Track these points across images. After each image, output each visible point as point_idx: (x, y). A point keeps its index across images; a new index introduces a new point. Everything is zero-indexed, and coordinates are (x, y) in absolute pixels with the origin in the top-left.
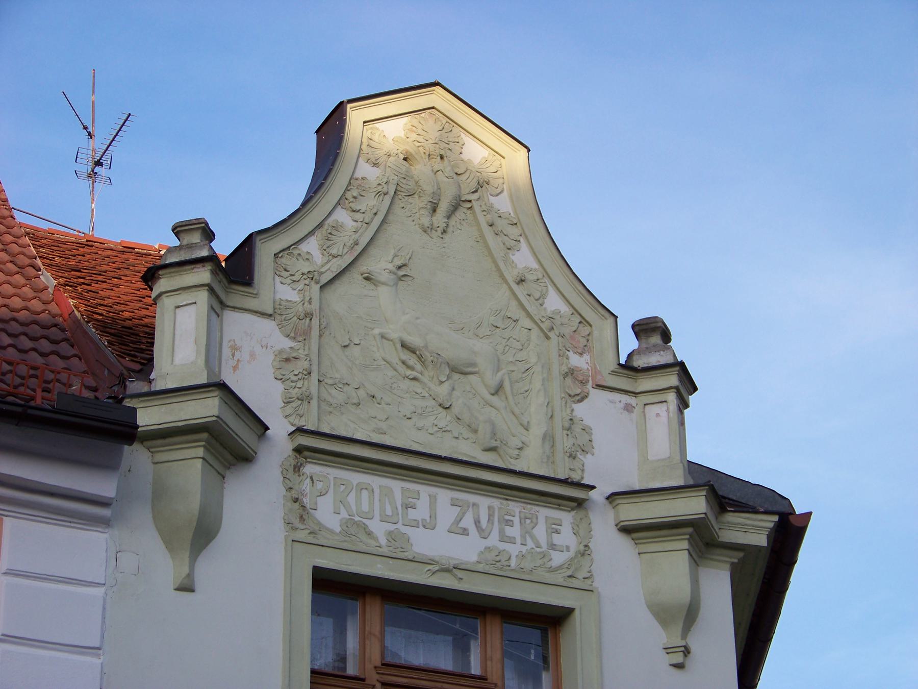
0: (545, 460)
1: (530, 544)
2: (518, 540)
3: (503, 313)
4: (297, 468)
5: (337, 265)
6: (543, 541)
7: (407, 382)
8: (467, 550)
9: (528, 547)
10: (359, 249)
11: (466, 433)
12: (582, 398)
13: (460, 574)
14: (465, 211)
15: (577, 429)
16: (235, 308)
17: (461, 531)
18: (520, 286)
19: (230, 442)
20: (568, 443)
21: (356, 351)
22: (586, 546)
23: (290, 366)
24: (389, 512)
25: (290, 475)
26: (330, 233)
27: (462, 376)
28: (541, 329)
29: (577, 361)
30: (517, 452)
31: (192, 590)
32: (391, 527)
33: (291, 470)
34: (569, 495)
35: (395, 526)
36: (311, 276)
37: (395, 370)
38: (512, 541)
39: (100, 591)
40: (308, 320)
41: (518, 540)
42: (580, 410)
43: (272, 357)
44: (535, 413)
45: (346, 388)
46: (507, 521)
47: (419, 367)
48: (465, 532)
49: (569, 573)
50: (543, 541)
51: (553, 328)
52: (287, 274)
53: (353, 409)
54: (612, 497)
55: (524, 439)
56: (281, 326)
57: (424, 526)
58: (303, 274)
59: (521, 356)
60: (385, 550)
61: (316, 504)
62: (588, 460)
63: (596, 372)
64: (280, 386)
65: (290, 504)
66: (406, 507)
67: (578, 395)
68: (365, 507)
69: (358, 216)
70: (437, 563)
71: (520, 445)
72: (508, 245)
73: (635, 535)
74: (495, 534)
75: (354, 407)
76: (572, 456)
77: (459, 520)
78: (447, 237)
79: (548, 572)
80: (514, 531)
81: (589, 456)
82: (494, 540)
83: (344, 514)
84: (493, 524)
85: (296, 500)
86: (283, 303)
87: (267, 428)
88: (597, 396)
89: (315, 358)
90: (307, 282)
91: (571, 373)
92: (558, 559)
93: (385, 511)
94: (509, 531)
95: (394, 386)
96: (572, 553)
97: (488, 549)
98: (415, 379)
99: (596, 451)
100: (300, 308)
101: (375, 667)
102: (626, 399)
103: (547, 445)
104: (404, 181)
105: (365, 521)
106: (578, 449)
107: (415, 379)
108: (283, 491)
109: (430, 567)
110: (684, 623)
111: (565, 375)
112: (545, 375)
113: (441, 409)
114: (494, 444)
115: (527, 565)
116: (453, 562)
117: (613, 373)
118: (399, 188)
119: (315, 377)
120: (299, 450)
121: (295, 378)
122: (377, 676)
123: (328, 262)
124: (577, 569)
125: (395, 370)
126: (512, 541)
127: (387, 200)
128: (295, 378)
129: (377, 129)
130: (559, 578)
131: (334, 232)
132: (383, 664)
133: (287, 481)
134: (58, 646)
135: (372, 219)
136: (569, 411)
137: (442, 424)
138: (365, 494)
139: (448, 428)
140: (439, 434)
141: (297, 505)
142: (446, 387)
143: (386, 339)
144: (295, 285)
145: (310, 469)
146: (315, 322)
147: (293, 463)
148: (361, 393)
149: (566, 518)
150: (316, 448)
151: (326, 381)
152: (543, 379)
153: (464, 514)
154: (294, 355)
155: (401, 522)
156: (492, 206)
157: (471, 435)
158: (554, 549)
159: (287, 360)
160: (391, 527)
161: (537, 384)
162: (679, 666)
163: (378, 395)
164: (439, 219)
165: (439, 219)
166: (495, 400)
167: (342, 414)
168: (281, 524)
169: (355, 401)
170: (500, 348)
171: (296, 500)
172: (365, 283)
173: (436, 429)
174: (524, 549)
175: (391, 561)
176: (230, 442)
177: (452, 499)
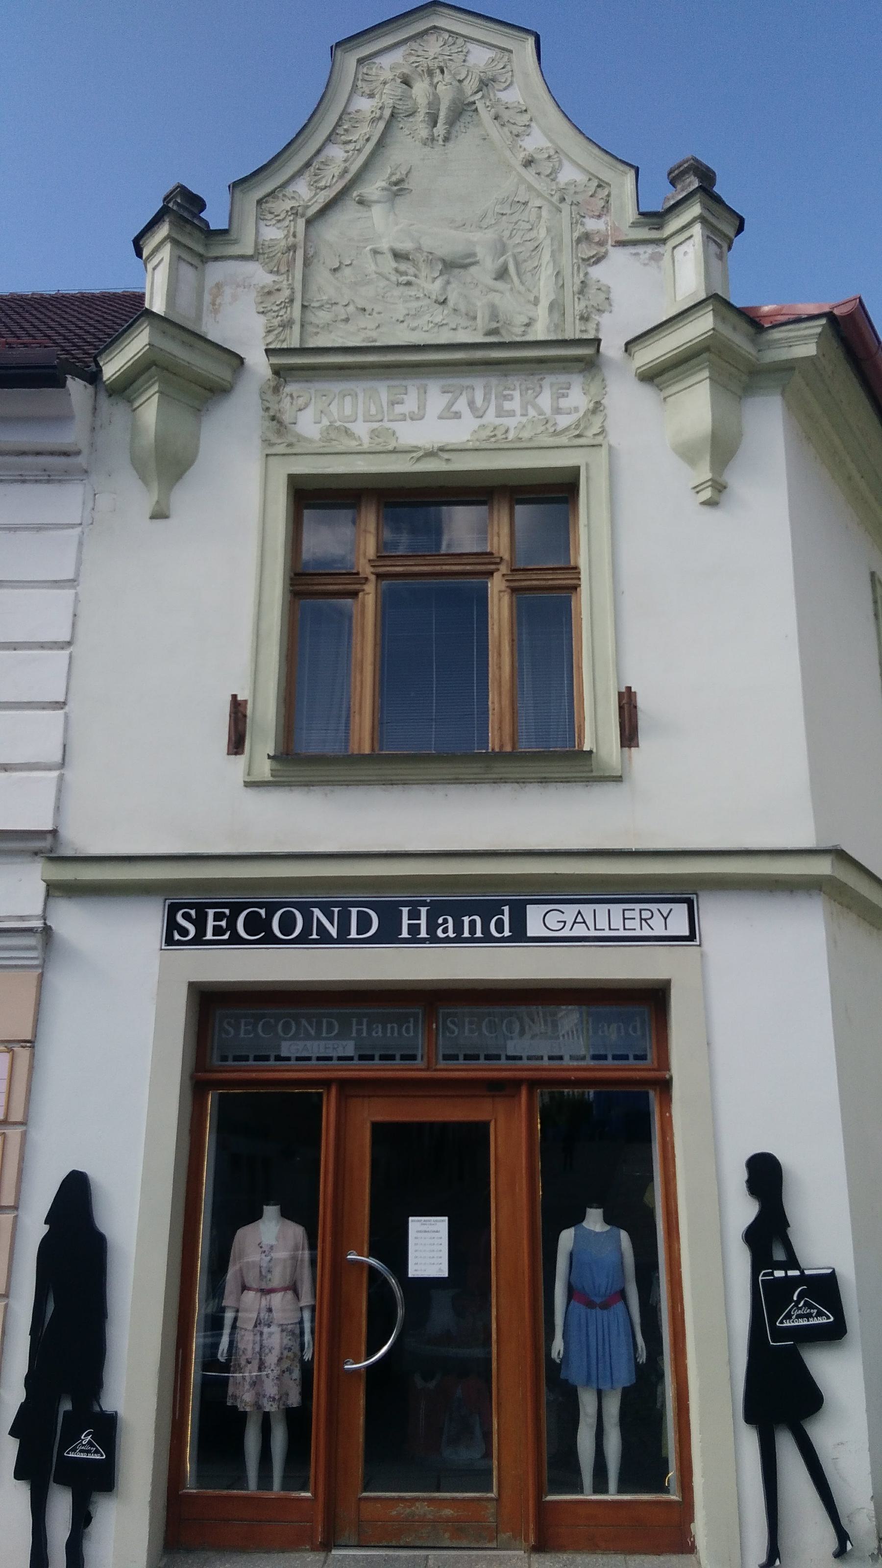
0: (552, 329)
1: (532, 412)
2: (518, 413)
3: (510, 200)
4: (276, 390)
5: (324, 197)
6: (548, 410)
7: (401, 288)
8: (460, 431)
9: (530, 417)
10: (348, 177)
11: (464, 322)
12: (598, 259)
13: (446, 456)
14: (471, 113)
15: (592, 291)
16: (216, 259)
17: (453, 415)
18: (529, 169)
19: (199, 377)
20: (580, 307)
21: (347, 271)
22: (597, 403)
23: (272, 299)
24: (373, 411)
25: (269, 396)
26: (318, 169)
27: (462, 270)
28: (551, 202)
29: (592, 225)
30: (523, 329)
31: (165, 516)
32: (375, 425)
33: (270, 392)
34: (579, 357)
35: (380, 424)
36: (295, 212)
37: (388, 279)
38: (511, 414)
39: (78, 530)
40: (291, 253)
41: (518, 413)
42: (596, 272)
43: (254, 294)
44: (545, 289)
45: (334, 307)
46: (505, 396)
47: (412, 270)
48: (457, 415)
49: (577, 432)
50: (548, 410)
51: (564, 199)
52: (272, 216)
53: (342, 326)
54: (629, 346)
55: (531, 314)
56: (264, 264)
57: (412, 419)
58: (287, 212)
59: (533, 234)
60: (366, 446)
61: (296, 418)
62: (605, 320)
63: (616, 229)
64: (262, 319)
65: (267, 423)
66: (393, 403)
67: (593, 257)
68: (348, 411)
69: (351, 147)
70: (420, 448)
71: (527, 321)
72: (515, 132)
73: (657, 381)
74: (492, 410)
75: (344, 323)
76: (584, 318)
77: (451, 404)
78: (450, 145)
79: (551, 436)
80: (515, 404)
81: (606, 315)
82: (490, 417)
83: (325, 422)
84: (489, 402)
85: (273, 418)
86: (266, 243)
87: (241, 360)
88: (618, 257)
89: (298, 286)
90: (291, 218)
91: (586, 237)
92: (563, 421)
93: (369, 411)
94: (507, 406)
95: (389, 294)
96: (581, 414)
97: (483, 427)
98: (409, 284)
99: (615, 309)
100: (283, 243)
101: (370, 561)
102: (650, 249)
103: (556, 316)
104: (401, 102)
105: (346, 425)
106: (594, 310)
107: (409, 284)
108: (262, 413)
109: (414, 455)
110: (712, 456)
111: (579, 241)
112: (555, 247)
113: (437, 305)
114: (494, 325)
115: (525, 435)
116: (436, 446)
117: (634, 225)
118: (396, 111)
119: (297, 305)
120: (277, 371)
121: (276, 308)
122: (372, 570)
123: (316, 194)
124: (586, 428)
125: (388, 279)
126: (511, 414)
127: (381, 125)
128: (276, 308)
129: (374, 63)
130: (564, 440)
131: (322, 167)
132: (378, 557)
133: (265, 402)
134: (36, 584)
135: (364, 146)
136: (582, 275)
137: (438, 319)
138: (348, 399)
139: (444, 322)
140: (436, 330)
141: (275, 422)
142: (439, 283)
143: (379, 253)
144: (279, 225)
145: (291, 388)
146: (300, 254)
147: (272, 384)
148: (351, 308)
149: (577, 381)
150: (295, 366)
151: (313, 304)
152: (552, 251)
153: (456, 399)
154: (276, 287)
155: (386, 419)
156: (499, 100)
157: (470, 323)
158: (561, 414)
159: (269, 293)
160: (375, 425)
161: (546, 256)
162: (711, 503)
163: (368, 308)
164: (440, 129)
165: (440, 129)
166: (499, 285)
167: (331, 332)
168: (257, 442)
169: (343, 317)
170: (507, 233)
171: (273, 418)
172: (360, 207)
173: (431, 325)
174: (524, 420)
175: (371, 456)
176: (199, 377)
177: (443, 387)
